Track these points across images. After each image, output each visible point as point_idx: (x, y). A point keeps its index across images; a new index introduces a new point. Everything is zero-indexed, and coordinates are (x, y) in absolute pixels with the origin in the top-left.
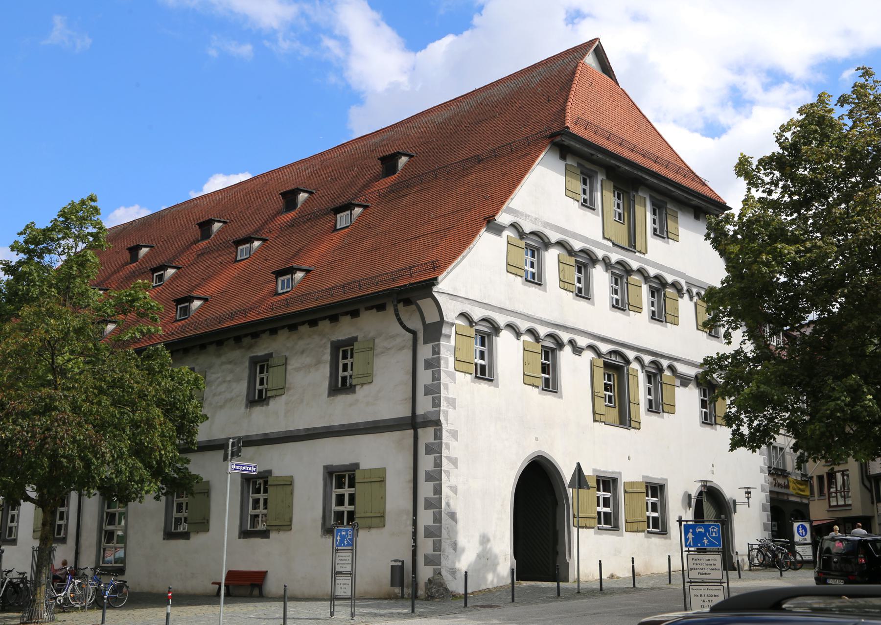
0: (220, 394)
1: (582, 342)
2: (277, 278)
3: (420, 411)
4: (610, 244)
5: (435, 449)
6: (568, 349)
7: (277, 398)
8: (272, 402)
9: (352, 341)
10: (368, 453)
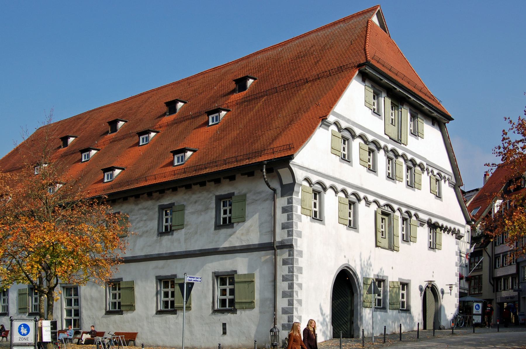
0: (139, 228)
1: (371, 198)
2: (174, 156)
3: (278, 239)
4: (388, 138)
5: (289, 262)
6: (363, 202)
7: (179, 231)
8: (175, 233)
9: (230, 196)
10: (240, 265)
